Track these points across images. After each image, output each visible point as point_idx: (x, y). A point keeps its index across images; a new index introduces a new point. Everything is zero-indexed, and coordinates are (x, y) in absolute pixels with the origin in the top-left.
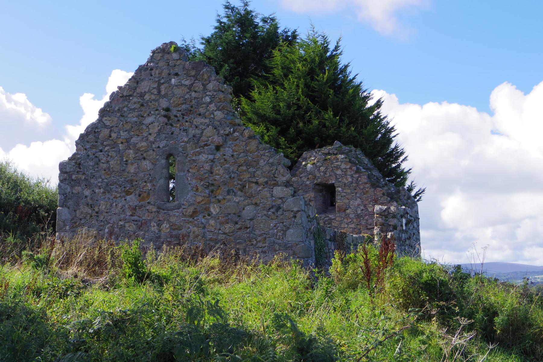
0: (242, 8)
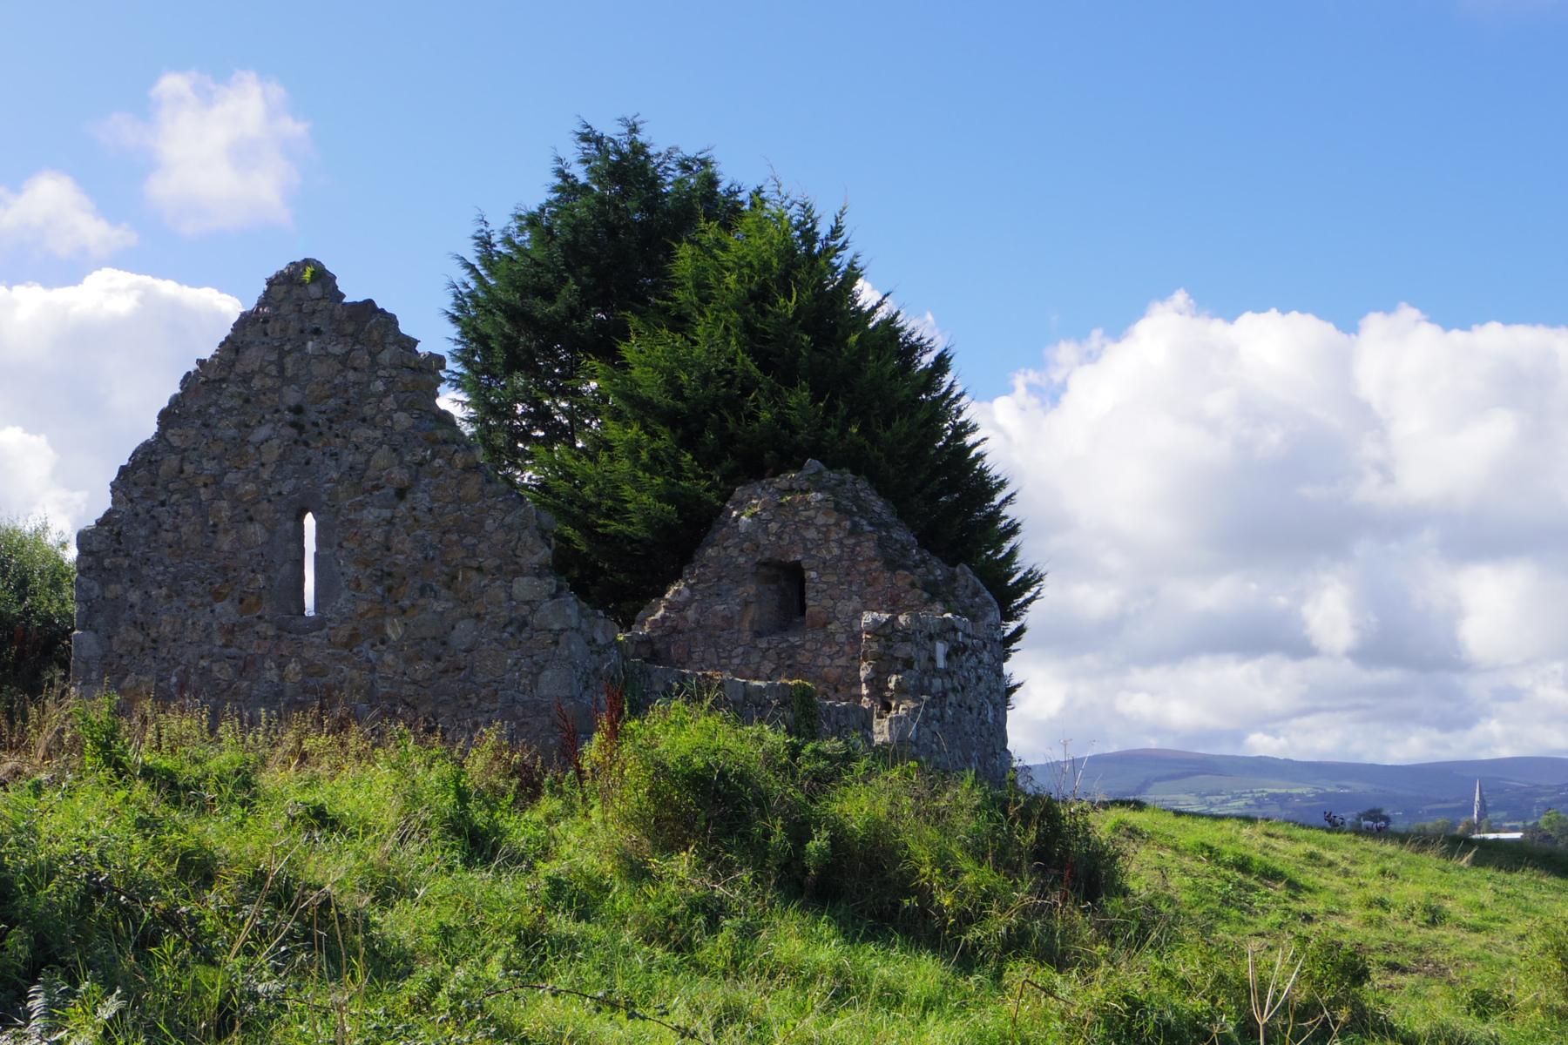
0: (625, 139)
